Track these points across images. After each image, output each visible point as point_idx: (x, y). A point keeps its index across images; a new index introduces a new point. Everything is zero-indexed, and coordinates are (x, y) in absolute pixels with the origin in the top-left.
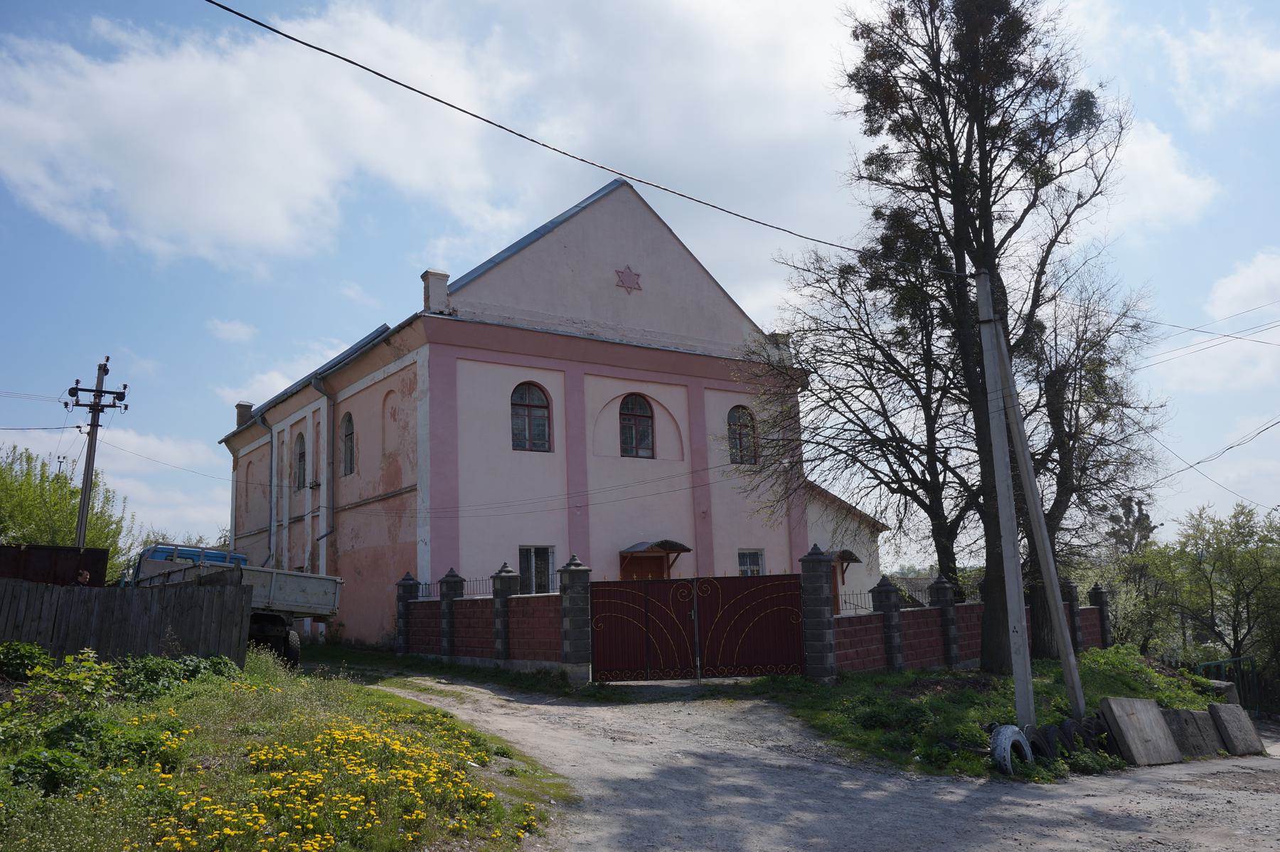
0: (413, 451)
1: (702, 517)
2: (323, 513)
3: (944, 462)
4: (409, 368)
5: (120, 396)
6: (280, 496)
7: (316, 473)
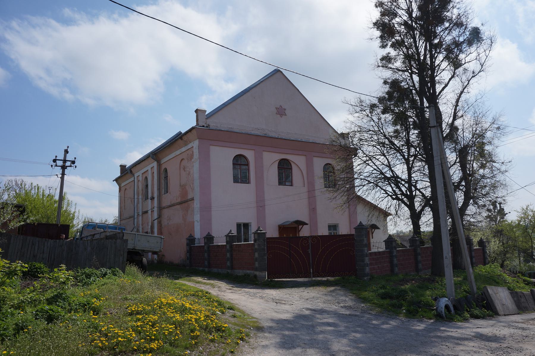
0: (192, 184)
1: (313, 210)
2: (156, 209)
3: (415, 187)
4: (190, 149)
5: (73, 162)
6: (138, 203)
7: (153, 193)
